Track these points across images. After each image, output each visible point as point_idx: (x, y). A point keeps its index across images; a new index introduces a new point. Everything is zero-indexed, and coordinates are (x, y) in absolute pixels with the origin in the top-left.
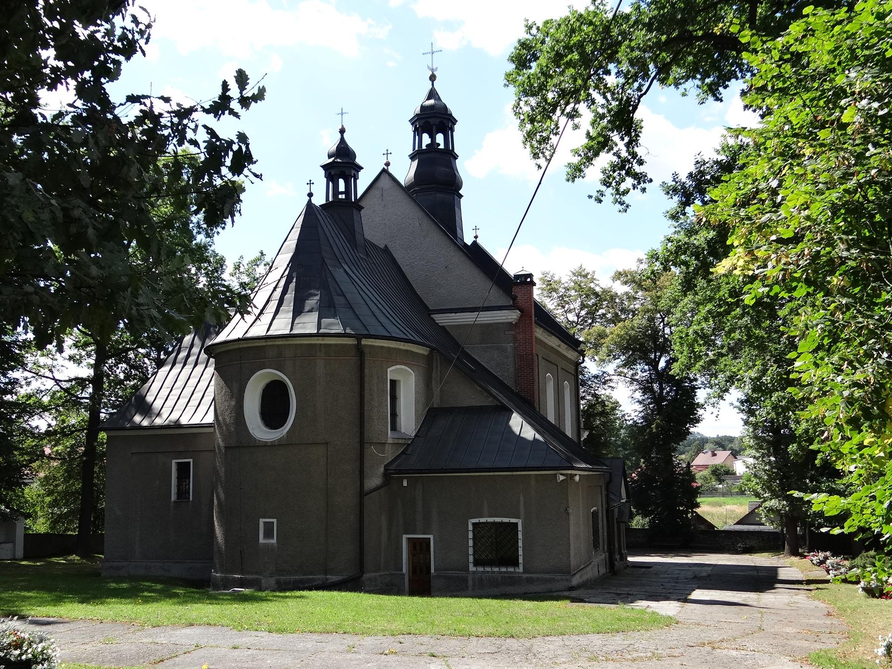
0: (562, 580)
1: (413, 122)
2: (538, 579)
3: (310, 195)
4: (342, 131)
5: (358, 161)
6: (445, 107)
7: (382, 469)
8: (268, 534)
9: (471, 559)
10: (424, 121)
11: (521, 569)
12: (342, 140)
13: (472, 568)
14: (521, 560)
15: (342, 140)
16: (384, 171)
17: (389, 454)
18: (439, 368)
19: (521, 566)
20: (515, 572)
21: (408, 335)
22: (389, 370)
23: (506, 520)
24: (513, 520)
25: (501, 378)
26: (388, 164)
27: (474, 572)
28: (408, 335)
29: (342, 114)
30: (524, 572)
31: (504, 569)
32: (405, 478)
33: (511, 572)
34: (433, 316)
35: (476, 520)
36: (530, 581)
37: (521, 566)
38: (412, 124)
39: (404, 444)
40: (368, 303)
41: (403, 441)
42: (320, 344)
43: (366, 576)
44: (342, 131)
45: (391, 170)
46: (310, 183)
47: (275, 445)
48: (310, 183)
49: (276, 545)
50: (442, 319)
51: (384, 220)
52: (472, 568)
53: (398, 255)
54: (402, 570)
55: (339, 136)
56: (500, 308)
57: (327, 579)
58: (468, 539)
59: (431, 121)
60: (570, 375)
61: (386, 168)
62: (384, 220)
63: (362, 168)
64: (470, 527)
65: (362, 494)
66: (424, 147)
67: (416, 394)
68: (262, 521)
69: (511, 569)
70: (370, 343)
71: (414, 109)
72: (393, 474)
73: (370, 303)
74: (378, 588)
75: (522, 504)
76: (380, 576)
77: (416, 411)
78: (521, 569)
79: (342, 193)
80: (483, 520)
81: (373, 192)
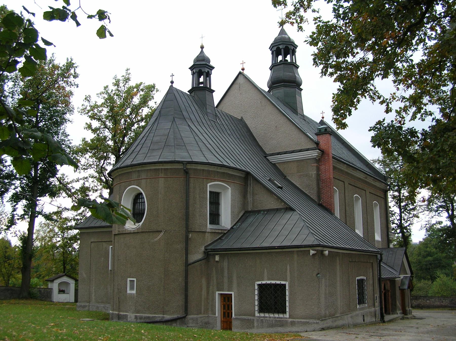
0: (314, 323)
1: (271, 48)
2: (298, 322)
3: (172, 82)
4: (202, 47)
5: (212, 64)
6: (289, 38)
7: (203, 249)
8: (132, 288)
9: (257, 308)
10: (276, 47)
11: (287, 315)
12: (202, 52)
13: (257, 314)
14: (287, 310)
15: (202, 52)
16: (240, 73)
17: (209, 239)
18: (252, 185)
19: (288, 313)
20: (284, 318)
21: (247, 168)
22: (208, 185)
23: (278, 282)
24: (283, 282)
25: (309, 194)
26: (243, 69)
27: (258, 317)
28: (247, 168)
29: (202, 37)
30: (290, 318)
31: (276, 315)
32: (217, 254)
33: (281, 318)
34: (268, 158)
35: (260, 283)
36: (293, 324)
37: (288, 313)
38: (271, 50)
39: (222, 233)
40: (199, 143)
41: (220, 231)
42: (162, 169)
43: (190, 317)
44: (202, 47)
45: (245, 72)
46: (172, 75)
47: (135, 233)
48: (172, 75)
49: (135, 295)
50: (272, 159)
51: (241, 102)
52: (257, 314)
53: (248, 122)
54: (215, 315)
55: (200, 50)
56: (308, 150)
57: (163, 317)
58: (254, 295)
59: (281, 47)
60: (381, 199)
61: (242, 71)
62: (241, 102)
63: (214, 68)
64: (256, 287)
65: (187, 265)
66: (279, 62)
67: (232, 201)
68: (129, 279)
69: (281, 316)
70: (194, 167)
71: (272, 41)
72: (210, 252)
73: (200, 144)
74: (198, 325)
75: (288, 271)
76: (201, 317)
77: (232, 212)
78: (287, 315)
79: (202, 83)
80: (264, 282)
81: (235, 86)
